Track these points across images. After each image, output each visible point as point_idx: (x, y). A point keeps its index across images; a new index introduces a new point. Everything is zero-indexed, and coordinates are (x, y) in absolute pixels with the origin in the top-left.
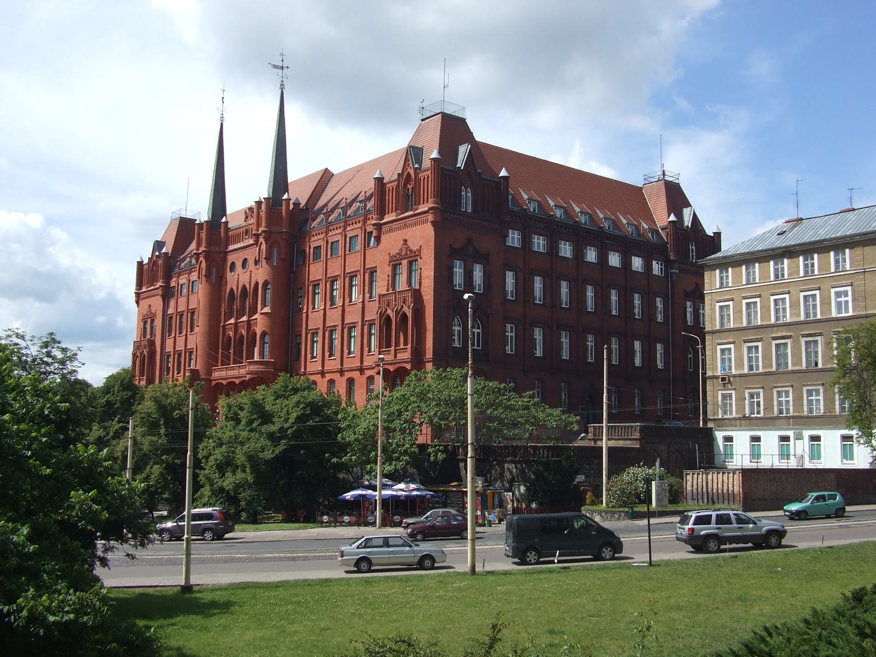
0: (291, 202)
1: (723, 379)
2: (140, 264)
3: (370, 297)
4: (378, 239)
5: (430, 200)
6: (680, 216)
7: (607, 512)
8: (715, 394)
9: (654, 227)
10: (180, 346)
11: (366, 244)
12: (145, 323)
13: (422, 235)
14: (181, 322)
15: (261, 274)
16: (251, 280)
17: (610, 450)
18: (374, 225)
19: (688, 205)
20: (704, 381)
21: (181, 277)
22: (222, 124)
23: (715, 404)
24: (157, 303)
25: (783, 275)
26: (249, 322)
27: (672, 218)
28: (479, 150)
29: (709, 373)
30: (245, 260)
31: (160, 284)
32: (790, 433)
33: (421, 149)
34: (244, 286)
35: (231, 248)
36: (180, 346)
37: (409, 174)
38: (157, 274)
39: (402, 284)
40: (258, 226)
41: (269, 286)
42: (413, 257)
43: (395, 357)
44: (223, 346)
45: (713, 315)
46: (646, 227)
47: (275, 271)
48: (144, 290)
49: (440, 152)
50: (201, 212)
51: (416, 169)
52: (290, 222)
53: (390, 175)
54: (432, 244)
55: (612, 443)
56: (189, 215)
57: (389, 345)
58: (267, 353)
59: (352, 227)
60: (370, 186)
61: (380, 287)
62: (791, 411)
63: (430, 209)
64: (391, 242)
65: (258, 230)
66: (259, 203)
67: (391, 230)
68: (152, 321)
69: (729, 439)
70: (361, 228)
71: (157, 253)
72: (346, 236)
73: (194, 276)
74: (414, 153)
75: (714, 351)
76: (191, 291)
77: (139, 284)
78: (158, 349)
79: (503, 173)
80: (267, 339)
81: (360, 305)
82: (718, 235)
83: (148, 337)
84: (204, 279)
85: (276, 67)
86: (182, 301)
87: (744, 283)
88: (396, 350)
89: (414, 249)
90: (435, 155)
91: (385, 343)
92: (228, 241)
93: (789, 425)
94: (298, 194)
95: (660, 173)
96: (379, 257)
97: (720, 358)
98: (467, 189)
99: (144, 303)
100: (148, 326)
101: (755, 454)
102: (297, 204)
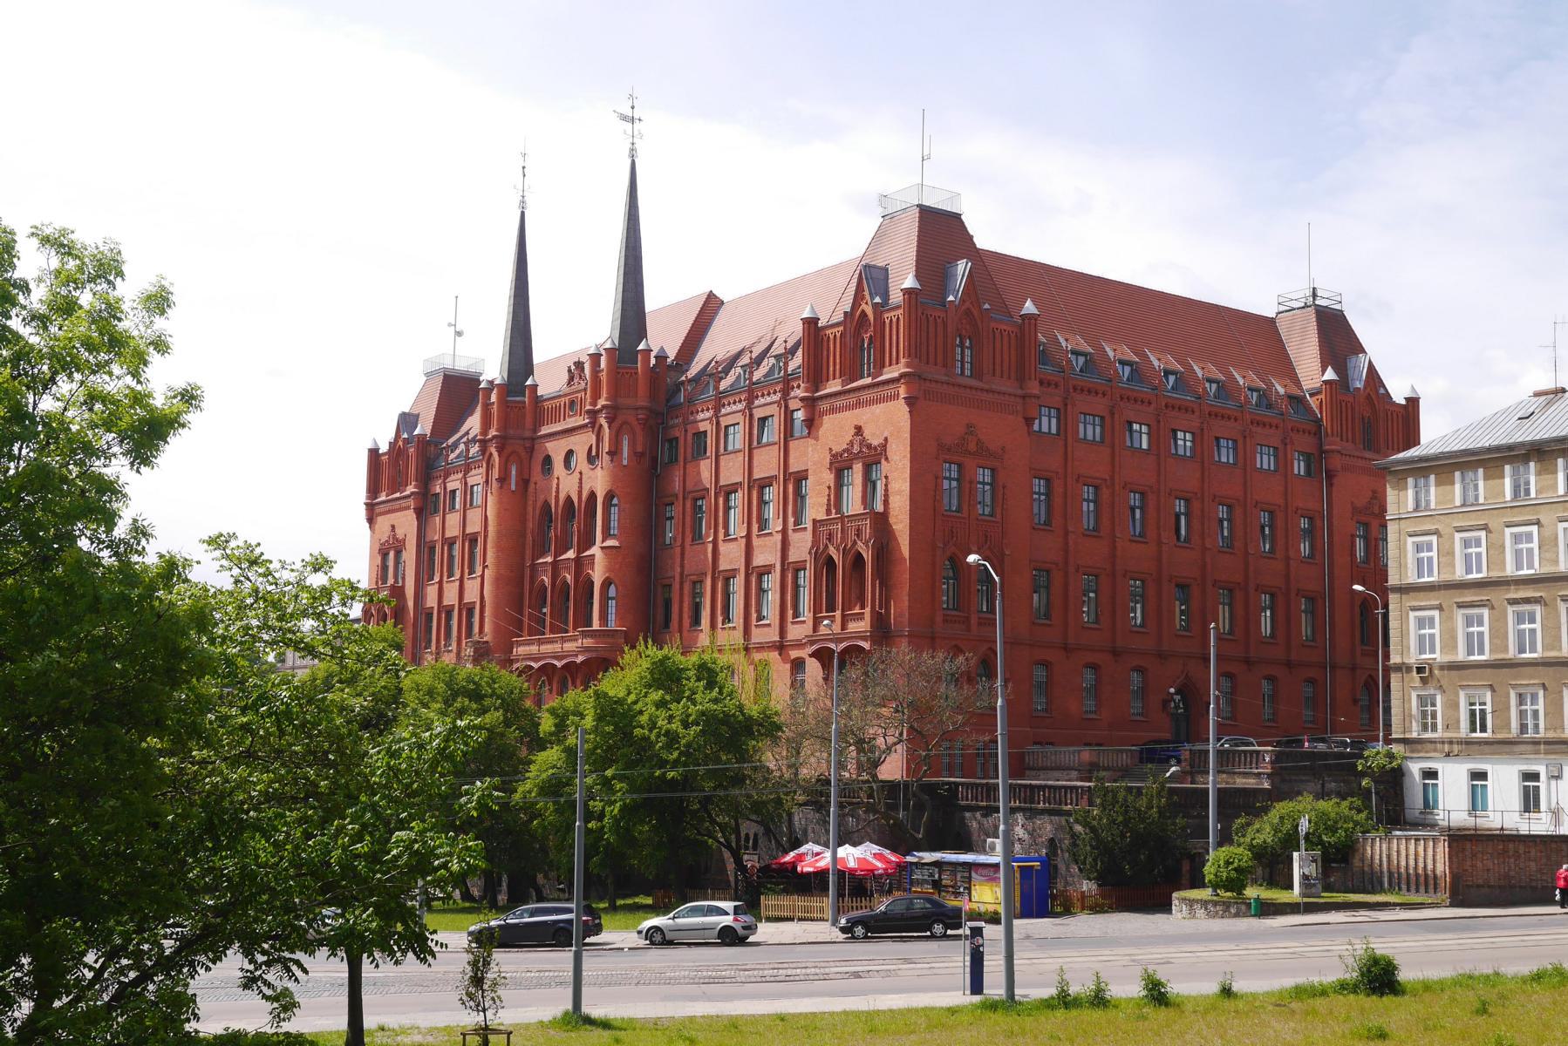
0: (653, 354)
1: (1420, 670)
2: (374, 454)
3: (796, 523)
4: (810, 423)
5: (903, 361)
6: (1341, 370)
7: (1215, 904)
8: (1405, 699)
9: (1295, 391)
10: (451, 598)
11: (788, 433)
12: (385, 556)
13: (889, 421)
14: (451, 557)
15: (599, 480)
16: (580, 487)
17: (1221, 793)
18: (802, 399)
19: (1359, 349)
20: (1387, 670)
21: (453, 477)
22: (523, 214)
23: (1407, 716)
24: (406, 523)
25: (1527, 492)
26: (578, 560)
27: (1330, 374)
28: (987, 264)
29: (1395, 659)
30: (570, 453)
31: (410, 489)
32: (1542, 770)
33: (885, 270)
34: (569, 499)
35: (545, 430)
36: (451, 598)
37: (864, 313)
38: (405, 472)
39: (853, 502)
40: (596, 396)
41: (615, 501)
42: (873, 457)
43: (844, 627)
44: (532, 599)
45: (1406, 558)
46: (1281, 391)
47: (618, 473)
48: (383, 498)
49: (918, 276)
50: (493, 369)
51: (875, 306)
52: (652, 395)
53: (832, 308)
54: (906, 435)
55: (1226, 782)
56: (462, 365)
57: (831, 607)
58: (612, 617)
59: (762, 401)
60: (793, 331)
61: (815, 508)
62: (1542, 725)
63: (902, 376)
64: (836, 430)
65: (594, 403)
66: (595, 358)
67: (833, 411)
68: (398, 553)
69: (1431, 774)
70: (778, 403)
71: (405, 436)
72: (751, 416)
73: (476, 477)
74: (871, 277)
75: (1404, 620)
76: (468, 504)
77: (373, 488)
78: (411, 604)
79: (1029, 307)
80: (612, 592)
81: (779, 537)
82: (1413, 402)
83: (391, 581)
84: (495, 485)
85: (624, 118)
86: (453, 520)
87: (1458, 503)
88: (843, 616)
89: (875, 442)
90: (910, 282)
91: (825, 603)
92: (538, 422)
93: (1537, 752)
94: (664, 338)
95: (1309, 293)
96: (812, 456)
97: (1415, 635)
98: (954, 318)
99: (383, 522)
100: (391, 563)
101: (1477, 800)
102: (661, 358)
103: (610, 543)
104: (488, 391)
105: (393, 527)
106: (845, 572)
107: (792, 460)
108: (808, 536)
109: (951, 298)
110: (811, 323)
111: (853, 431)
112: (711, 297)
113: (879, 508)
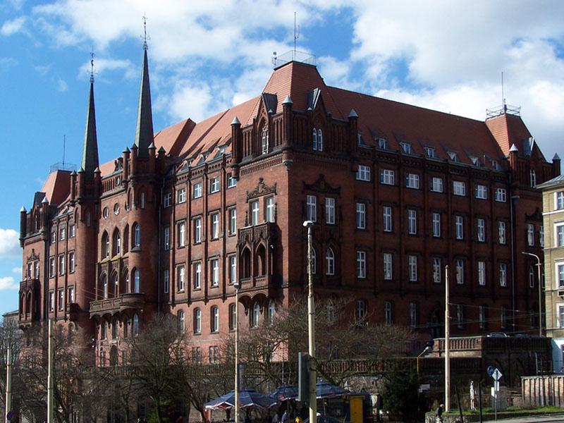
0: (157, 151)
2: (24, 213)
17: (452, 360)
24: (39, 247)
29: (548, 288)
33: (275, 96)
51: (269, 115)
75: (552, 267)
80: (137, 273)
82: (557, 162)
90: (286, 100)
94: (164, 141)
95: (502, 108)
102: (162, 151)
103: (135, 249)
104: (75, 175)
105: (33, 250)
106: (257, 252)
107: (227, 200)
108: (236, 239)
109: (310, 109)
110: (237, 127)
111: (259, 181)
112: (189, 120)
113: (271, 220)
